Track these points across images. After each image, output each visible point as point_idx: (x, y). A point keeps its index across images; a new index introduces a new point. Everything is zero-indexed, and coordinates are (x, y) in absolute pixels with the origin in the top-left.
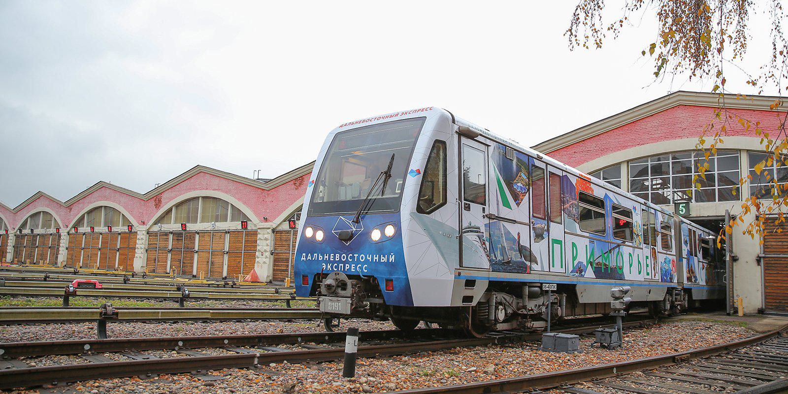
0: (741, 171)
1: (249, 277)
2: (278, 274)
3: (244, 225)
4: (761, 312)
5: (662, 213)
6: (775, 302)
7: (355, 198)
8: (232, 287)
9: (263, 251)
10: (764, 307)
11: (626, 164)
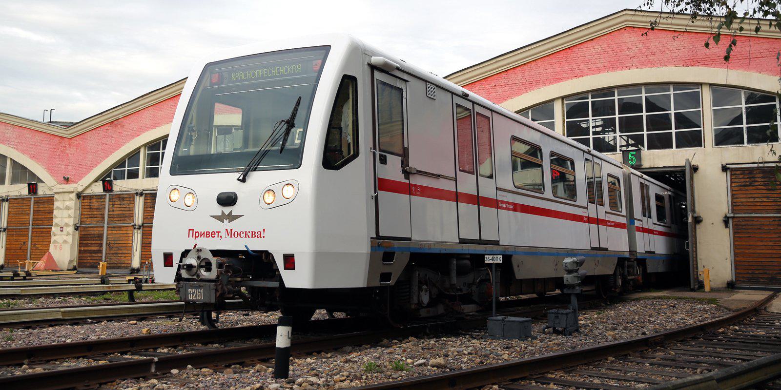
0: (703, 110)
1: (41, 264)
2: (86, 257)
3: (33, 189)
4: (731, 286)
5: (612, 164)
6: (746, 274)
7: (237, 149)
8: (25, 278)
9: (62, 224)
10: (734, 279)
11: (560, 101)
